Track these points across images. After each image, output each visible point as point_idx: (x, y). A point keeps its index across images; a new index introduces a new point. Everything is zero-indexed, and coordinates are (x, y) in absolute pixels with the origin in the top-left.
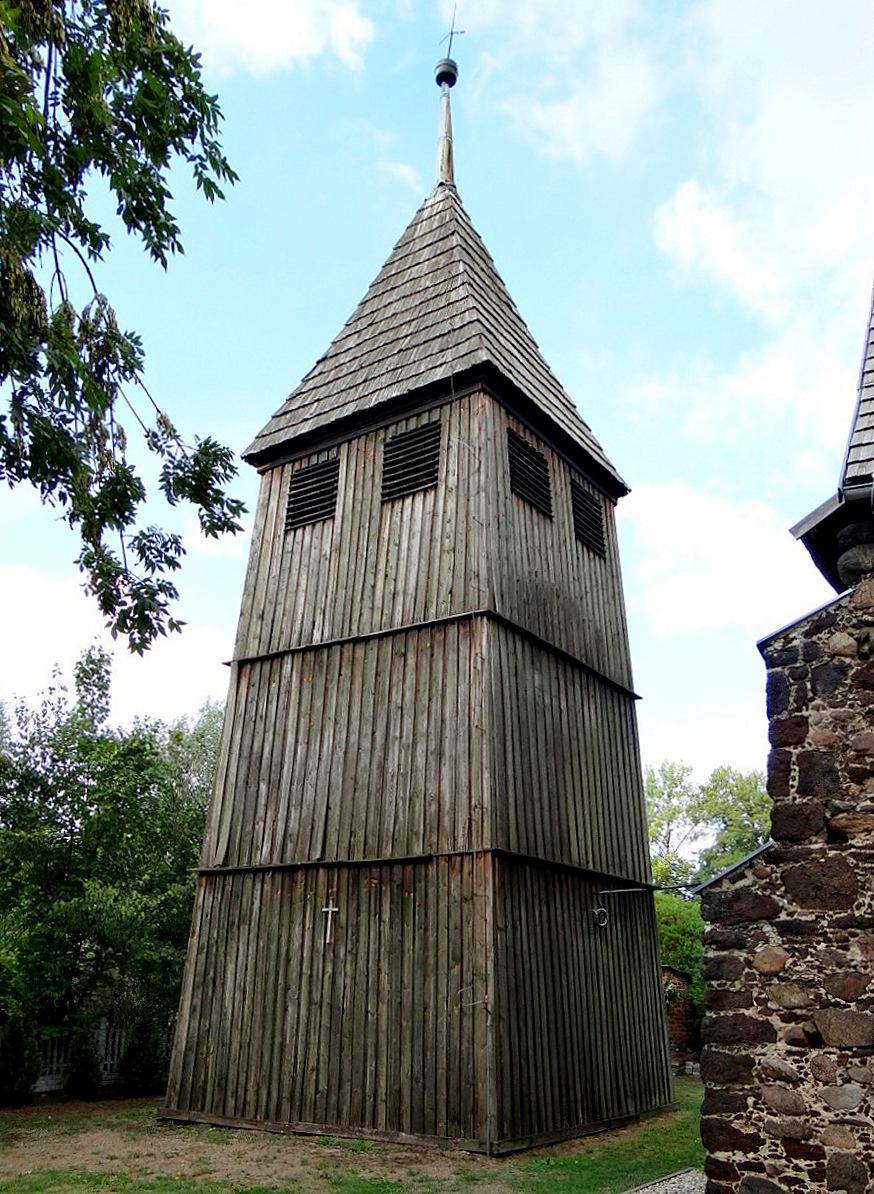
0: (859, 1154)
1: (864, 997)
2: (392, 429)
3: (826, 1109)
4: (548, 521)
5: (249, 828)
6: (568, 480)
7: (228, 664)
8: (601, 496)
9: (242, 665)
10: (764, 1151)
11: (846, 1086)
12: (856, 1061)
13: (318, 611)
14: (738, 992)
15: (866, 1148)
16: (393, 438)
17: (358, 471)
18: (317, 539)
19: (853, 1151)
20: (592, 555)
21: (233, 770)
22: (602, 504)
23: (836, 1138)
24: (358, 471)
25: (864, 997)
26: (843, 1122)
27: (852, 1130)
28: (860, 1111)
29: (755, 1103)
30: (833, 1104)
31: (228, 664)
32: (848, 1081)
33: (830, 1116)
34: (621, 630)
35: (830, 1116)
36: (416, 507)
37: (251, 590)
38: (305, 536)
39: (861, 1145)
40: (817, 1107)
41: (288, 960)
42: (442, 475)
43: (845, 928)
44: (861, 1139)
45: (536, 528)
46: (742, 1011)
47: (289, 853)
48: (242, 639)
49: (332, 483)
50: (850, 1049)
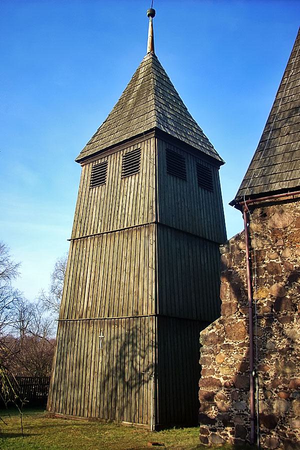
0: (245, 425)
1: (247, 371)
2: (125, 151)
3: (235, 410)
4: (185, 182)
5: (75, 305)
6: (195, 163)
7: (70, 240)
8: (212, 167)
9: (73, 240)
10: (217, 425)
11: (242, 402)
12: (244, 393)
13: (99, 221)
14: (211, 369)
15: (247, 423)
16: (125, 154)
17: (115, 164)
18: (99, 192)
19: (243, 424)
20: (206, 191)
21: (70, 282)
22: (212, 170)
23: (238, 420)
24: (115, 164)
25: (247, 371)
26: (240, 414)
27: (243, 417)
28: (245, 410)
29: (215, 408)
30: (237, 408)
31: (70, 240)
32: (242, 400)
33: (236, 412)
34: (221, 220)
35: (236, 412)
36: (132, 180)
37: (77, 213)
38: (96, 190)
39: (245, 422)
40: (232, 409)
41: (87, 356)
42: (141, 168)
43: (242, 347)
44: (245, 420)
45: (178, 186)
46: (212, 376)
47: (88, 315)
48: (74, 231)
49: (106, 168)
50: (243, 389)
